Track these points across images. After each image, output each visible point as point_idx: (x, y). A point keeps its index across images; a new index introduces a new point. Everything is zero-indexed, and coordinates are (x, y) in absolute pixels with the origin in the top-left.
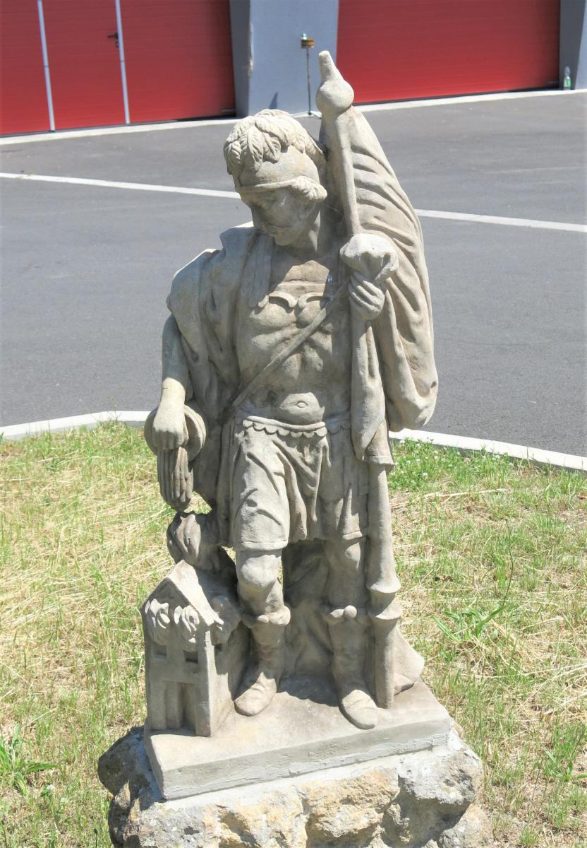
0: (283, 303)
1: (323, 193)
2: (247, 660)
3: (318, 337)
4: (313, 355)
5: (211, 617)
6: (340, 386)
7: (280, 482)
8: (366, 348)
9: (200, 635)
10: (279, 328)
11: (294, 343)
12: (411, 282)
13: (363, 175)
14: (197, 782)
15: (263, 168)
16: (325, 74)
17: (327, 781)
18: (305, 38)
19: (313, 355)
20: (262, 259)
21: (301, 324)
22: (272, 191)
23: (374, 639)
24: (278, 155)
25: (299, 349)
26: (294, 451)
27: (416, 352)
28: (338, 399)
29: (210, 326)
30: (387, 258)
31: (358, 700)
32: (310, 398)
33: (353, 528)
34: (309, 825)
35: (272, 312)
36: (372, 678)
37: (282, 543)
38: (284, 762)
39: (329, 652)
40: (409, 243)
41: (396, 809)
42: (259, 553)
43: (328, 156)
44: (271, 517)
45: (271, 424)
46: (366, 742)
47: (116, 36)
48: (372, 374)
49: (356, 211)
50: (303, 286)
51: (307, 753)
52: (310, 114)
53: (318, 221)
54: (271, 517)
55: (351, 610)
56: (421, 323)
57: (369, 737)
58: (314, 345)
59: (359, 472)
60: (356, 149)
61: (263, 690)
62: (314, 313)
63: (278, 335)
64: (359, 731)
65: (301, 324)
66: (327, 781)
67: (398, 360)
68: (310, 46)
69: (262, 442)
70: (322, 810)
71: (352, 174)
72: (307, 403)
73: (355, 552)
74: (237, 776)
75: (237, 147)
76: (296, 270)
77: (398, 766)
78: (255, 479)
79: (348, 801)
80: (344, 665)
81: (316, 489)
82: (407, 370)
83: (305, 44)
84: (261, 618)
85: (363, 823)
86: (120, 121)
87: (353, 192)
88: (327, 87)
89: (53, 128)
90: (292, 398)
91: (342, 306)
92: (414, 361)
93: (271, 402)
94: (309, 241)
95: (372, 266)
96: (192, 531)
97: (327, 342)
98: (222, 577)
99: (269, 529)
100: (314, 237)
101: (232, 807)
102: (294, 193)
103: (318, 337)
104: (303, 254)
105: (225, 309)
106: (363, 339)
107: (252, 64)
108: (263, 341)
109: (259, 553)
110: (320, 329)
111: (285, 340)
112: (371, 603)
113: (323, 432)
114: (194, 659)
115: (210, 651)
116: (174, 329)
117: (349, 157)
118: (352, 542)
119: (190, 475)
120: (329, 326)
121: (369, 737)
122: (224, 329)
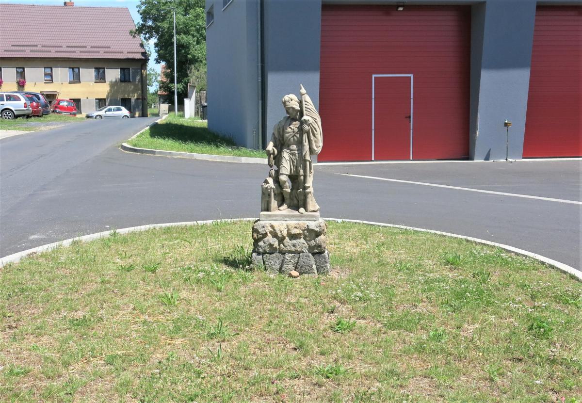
0: (291, 128)
1: (299, 109)
2: (282, 201)
3: (296, 135)
4: (295, 138)
5: (273, 186)
6: (300, 143)
7: (288, 162)
8: (305, 136)
9: (271, 190)
10: (289, 133)
11: (292, 136)
12: (316, 126)
13: (307, 106)
14: (267, 218)
15: (288, 103)
16: (301, 88)
17: (292, 223)
18: (506, 122)
19: (295, 138)
20: (289, 121)
21: (294, 132)
22: (289, 108)
23: (305, 196)
24: (290, 101)
25: (293, 137)
26: (291, 156)
27: (316, 140)
28: (300, 147)
29: (279, 132)
30: (308, 120)
31: (302, 210)
32: (295, 146)
33: (302, 172)
34: (287, 231)
35: (289, 130)
36: (305, 206)
37: (288, 173)
38: (284, 218)
39: (298, 202)
40: (315, 119)
41: (306, 231)
42: (283, 174)
43: (300, 103)
44: (286, 167)
45: (288, 151)
46: (301, 216)
47: (410, 117)
48: (306, 142)
49: (305, 112)
50: (295, 126)
51: (289, 216)
52: (507, 160)
53: (298, 114)
54: (286, 167)
55: (301, 190)
56: (317, 134)
57: (302, 216)
58: (295, 136)
59: (302, 161)
60: (305, 101)
61: (285, 206)
62: (296, 130)
63: (290, 134)
64: (299, 214)
65: (294, 132)
66: (292, 223)
67: (311, 140)
68: (509, 126)
69: (286, 154)
70: (290, 228)
71: (304, 106)
72: (294, 147)
73: (302, 178)
74: (274, 219)
75: (284, 100)
76: (294, 123)
77: (307, 223)
78: (284, 161)
79: (296, 228)
80: (301, 203)
81: (295, 164)
82: (314, 143)
83: (506, 124)
84: (284, 189)
85: (298, 232)
86: (409, 159)
87: (304, 109)
88: (301, 91)
89: (373, 159)
90: (292, 146)
91: (301, 130)
92: (315, 141)
93: (288, 147)
94: (296, 117)
95: (306, 122)
96: (273, 172)
97: (298, 136)
98: (277, 181)
99: (285, 170)
100: (298, 117)
101: (272, 224)
102: (293, 108)
103: (296, 135)
104: (296, 120)
105: (282, 129)
106: (304, 135)
107: (478, 133)
108: (287, 135)
109: (283, 174)
110: (297, 133)
111: (291, 135)
112: (305, 188)
113: (297, 153)
114: (269, 195)
115: (272, 194)
116: (274, 134)
117: (304, 103)
118: (302, 175)
119: (274, 161)
120: (298, 133)
121: (302, 216)
122: (281, 133)
